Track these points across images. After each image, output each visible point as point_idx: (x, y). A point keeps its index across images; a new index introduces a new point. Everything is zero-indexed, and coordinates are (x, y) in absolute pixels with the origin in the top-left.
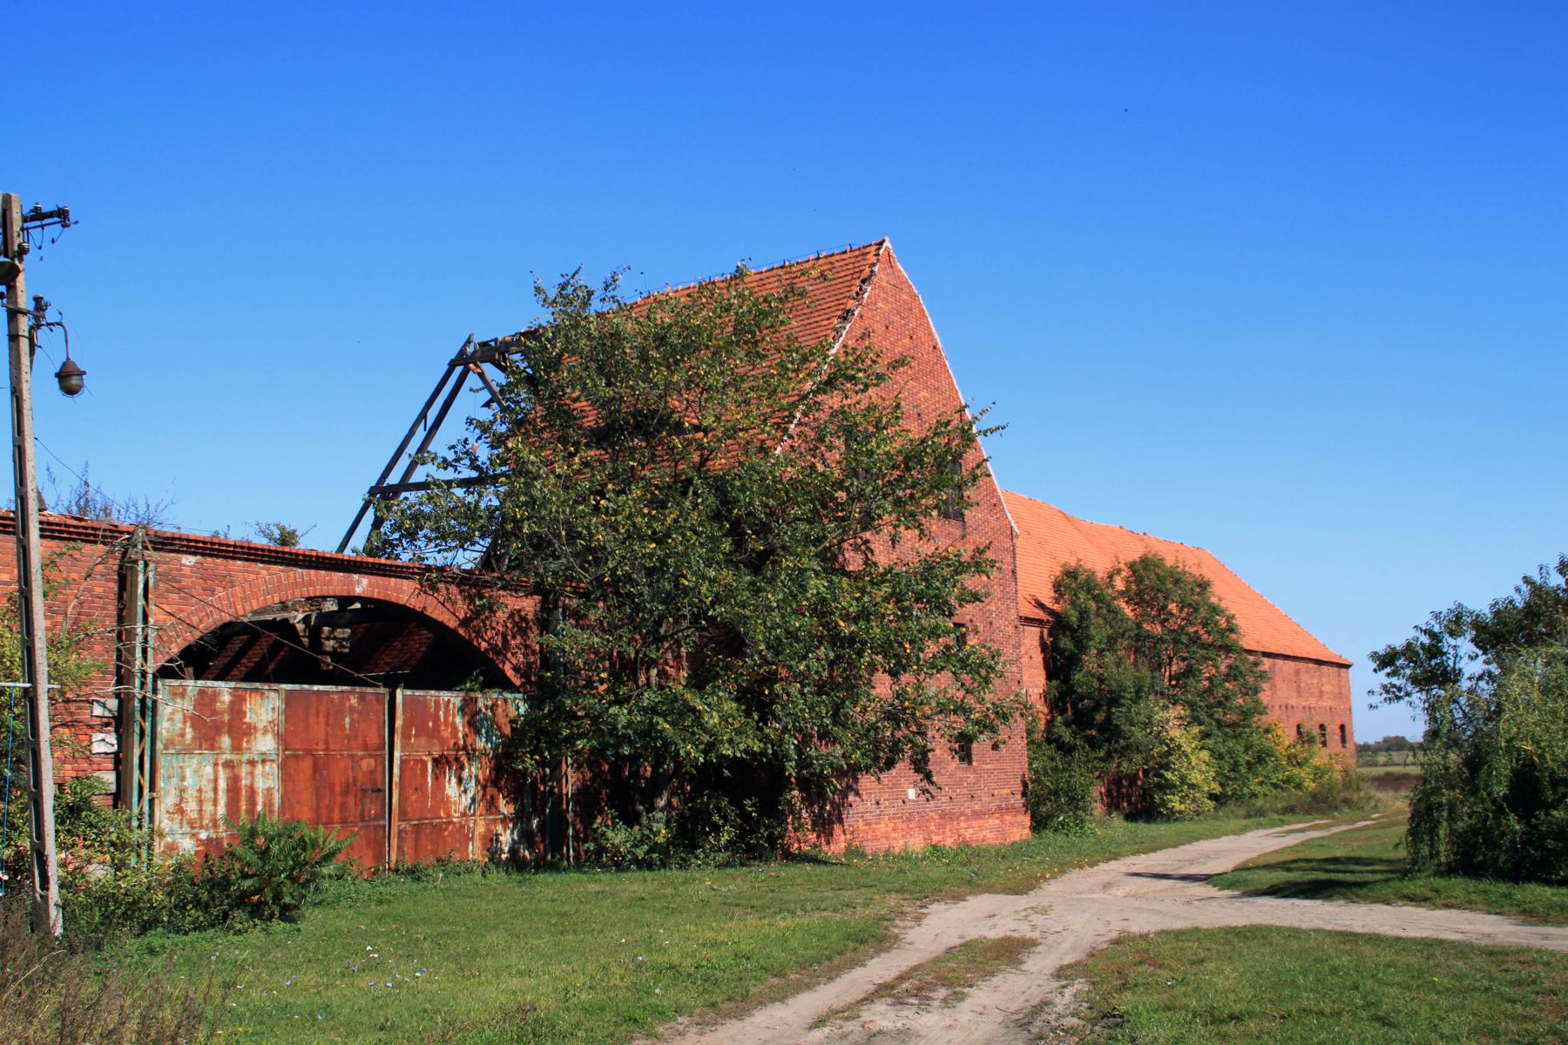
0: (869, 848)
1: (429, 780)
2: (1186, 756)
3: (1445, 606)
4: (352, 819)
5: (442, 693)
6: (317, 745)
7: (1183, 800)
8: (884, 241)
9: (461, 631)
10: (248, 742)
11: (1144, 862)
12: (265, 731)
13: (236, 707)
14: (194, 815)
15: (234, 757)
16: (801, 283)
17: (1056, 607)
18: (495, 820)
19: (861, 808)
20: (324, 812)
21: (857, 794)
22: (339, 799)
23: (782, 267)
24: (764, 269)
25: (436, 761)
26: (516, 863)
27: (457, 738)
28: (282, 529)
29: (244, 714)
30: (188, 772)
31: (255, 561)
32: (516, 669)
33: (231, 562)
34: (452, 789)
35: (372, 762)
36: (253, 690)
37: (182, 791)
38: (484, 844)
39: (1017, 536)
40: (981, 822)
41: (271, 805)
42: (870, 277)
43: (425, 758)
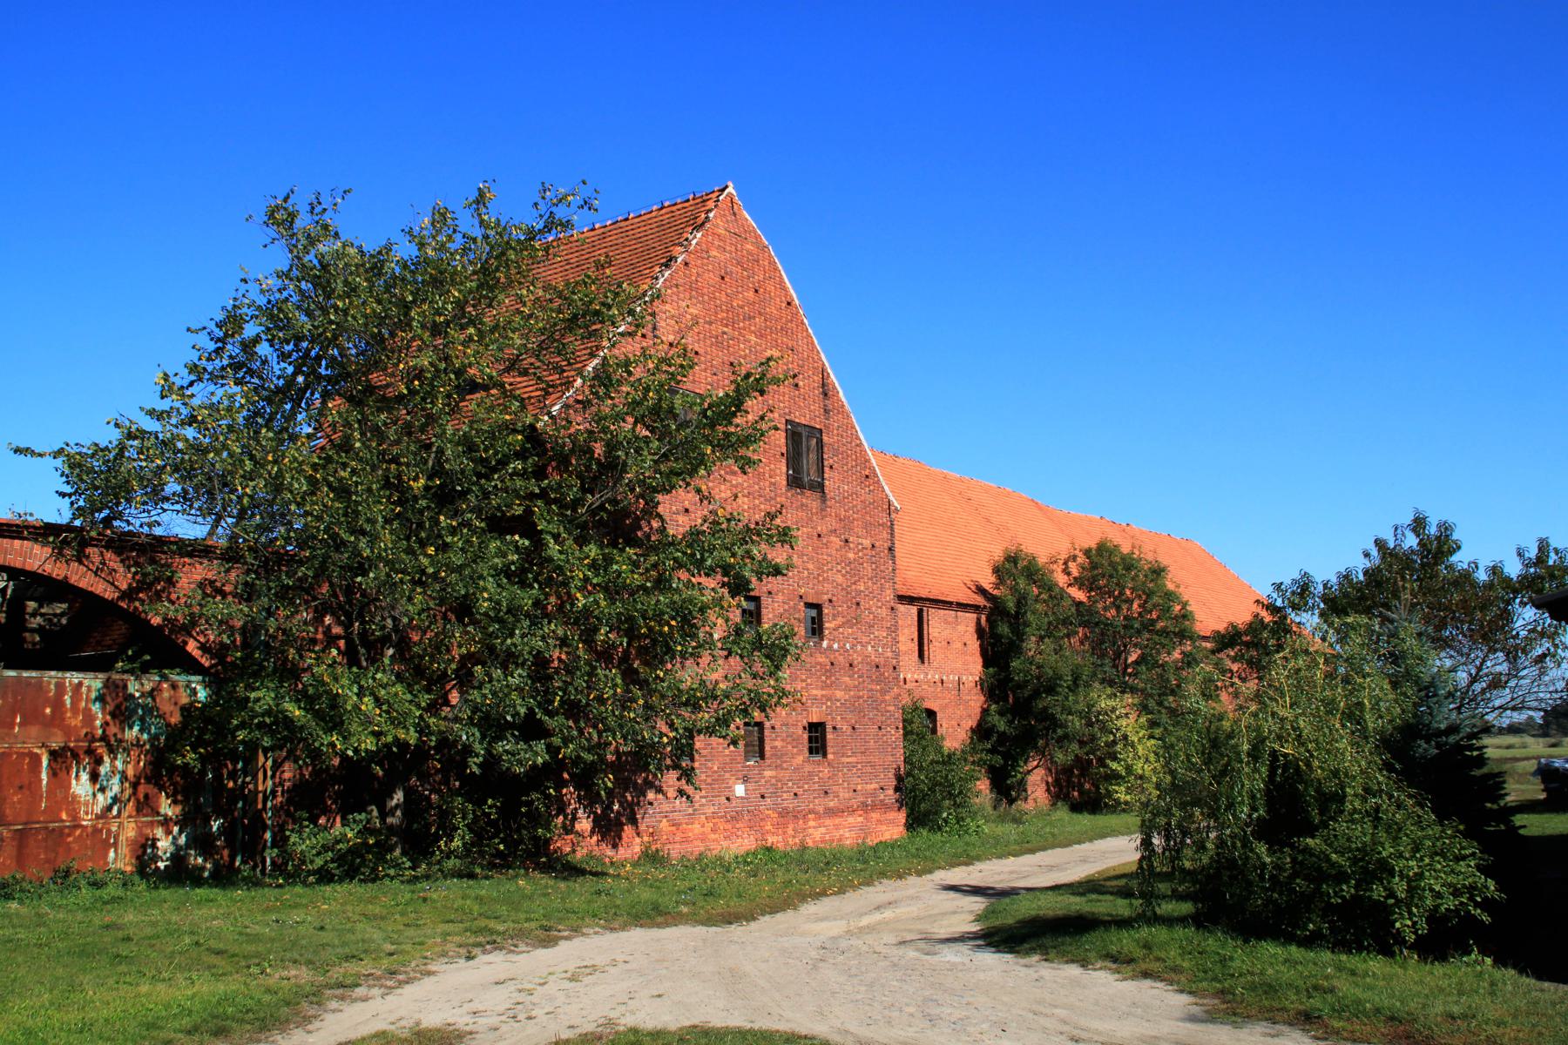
0: (675, 851)
1: (44, 776)
2: (1133, 746)
3: (1288, 576)
5: (68, 675)
7: (1129, 791)
8: (727, 187)
11: (958, 875)
16: (561, 213)
17: (996, 592)
18: (152, 823)
19: (666, 807)
23: (627, 219)
24: (609, 223)
25: (54, 755)
26: (179, 873)
27: (93, 728)
32: (204, 648)
34: (81, 786)
38: (133, 851)
39: (896, 510)
40: (837, 821)
42: (703, 224)
43: (37, 751)
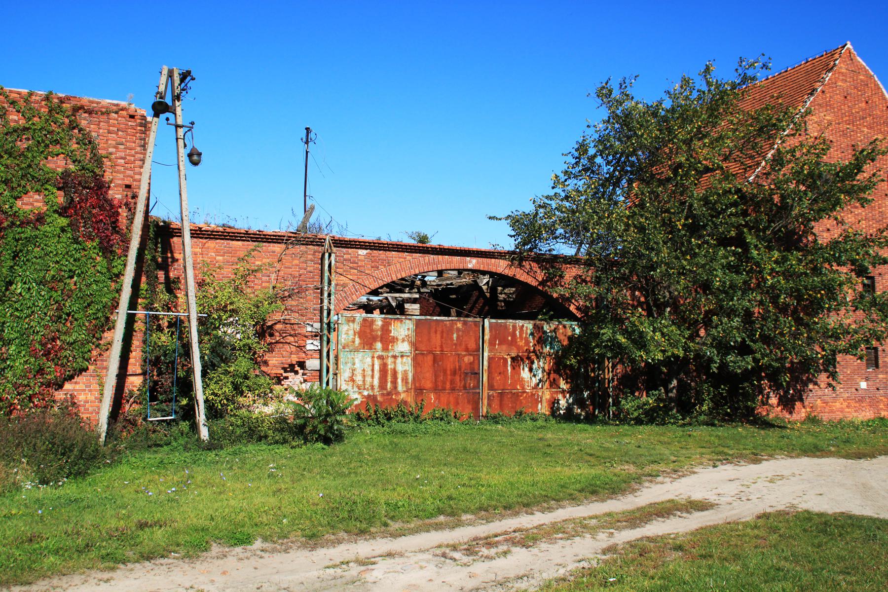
0: (825, 417)
1: (509, 368)
4: (458, 388)
5: (517, 321)
6: (436, 348)
8: (846, 45)
9: (540, 288)
10: (392, 346)
12: (403, 341)
13: (385, 328)
14: (360, 383)
15: (384, 354)
20: (440, 384)
21: (816, 384)
22: (449, 377)
23: (786, 71)
25: (513, 359)
26: (569, 417)
27: (529, 346)
28: (419, 235)
29: (391, 331)
30: (357, 361)
31: (404, 252)
32: (578, 308)
33: (388, 252)
34: (525, 374)
35: (472, 358)
36: (395, 319)
37: (353, 370)
41: (407, 379)
42: (832, 68)
43: (506, 357)
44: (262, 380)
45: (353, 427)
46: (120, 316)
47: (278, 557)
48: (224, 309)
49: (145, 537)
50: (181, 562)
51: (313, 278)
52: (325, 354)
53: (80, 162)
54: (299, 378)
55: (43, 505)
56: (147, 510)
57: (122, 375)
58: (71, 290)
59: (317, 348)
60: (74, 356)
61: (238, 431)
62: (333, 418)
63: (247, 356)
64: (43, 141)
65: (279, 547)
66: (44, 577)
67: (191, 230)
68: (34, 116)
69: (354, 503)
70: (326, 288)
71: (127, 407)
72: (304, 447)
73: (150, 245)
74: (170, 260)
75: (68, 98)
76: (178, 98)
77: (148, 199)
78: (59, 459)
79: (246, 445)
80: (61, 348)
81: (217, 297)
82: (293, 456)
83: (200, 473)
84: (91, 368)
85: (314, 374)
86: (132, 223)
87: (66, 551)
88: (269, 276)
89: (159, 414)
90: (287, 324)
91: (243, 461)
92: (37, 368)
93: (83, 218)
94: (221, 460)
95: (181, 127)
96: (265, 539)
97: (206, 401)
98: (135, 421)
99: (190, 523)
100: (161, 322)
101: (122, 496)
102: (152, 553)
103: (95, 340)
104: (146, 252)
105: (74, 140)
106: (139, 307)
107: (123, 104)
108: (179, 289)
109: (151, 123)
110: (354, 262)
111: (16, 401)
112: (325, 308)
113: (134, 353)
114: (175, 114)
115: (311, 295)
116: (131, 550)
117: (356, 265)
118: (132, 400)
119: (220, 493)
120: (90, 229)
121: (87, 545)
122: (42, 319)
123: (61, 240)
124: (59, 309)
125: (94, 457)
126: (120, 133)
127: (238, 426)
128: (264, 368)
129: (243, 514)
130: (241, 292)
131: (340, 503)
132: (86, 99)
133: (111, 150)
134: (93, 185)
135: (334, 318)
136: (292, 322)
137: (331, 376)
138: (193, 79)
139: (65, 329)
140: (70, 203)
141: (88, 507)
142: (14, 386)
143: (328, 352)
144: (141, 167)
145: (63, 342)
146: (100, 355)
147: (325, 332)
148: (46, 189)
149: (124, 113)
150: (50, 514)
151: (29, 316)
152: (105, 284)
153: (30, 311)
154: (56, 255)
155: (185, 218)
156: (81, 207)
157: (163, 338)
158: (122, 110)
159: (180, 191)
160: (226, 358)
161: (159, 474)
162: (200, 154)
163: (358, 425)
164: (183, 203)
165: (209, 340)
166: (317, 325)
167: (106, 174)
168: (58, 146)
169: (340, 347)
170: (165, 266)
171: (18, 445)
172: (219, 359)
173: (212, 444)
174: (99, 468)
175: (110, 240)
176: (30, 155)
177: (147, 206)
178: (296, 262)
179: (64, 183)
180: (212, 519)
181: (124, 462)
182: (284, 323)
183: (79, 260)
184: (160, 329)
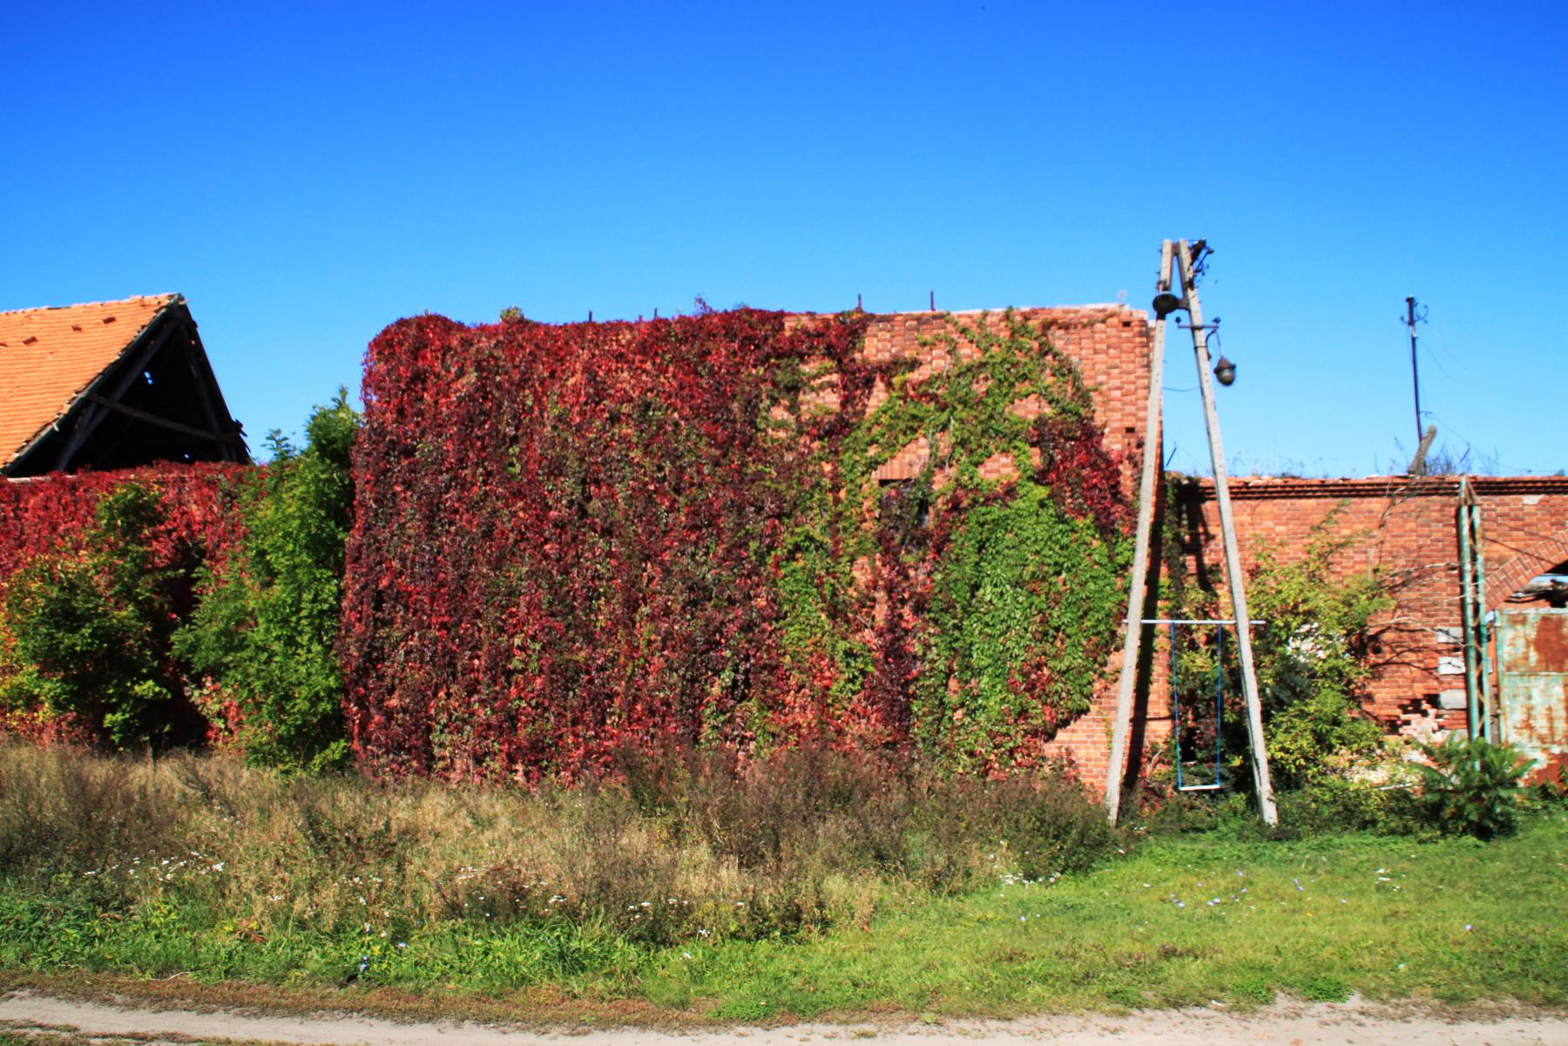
14: (1545, 731)
30: (1535, 692)
37: (1530, 708)
44: (1362, 727)
45: (1535, 811)
46: (1130, 627)
47: (1389, 1029)
48: (1294, 611)
49: (1172, 971)
50: (1226, 1017)
51: (1443, 550)
52: (1473, 681)
53: (1058, 402)
54: (1430, 722)
55: (1029, 909)
56: (1177, 931)
57: (1139, 720)
58: (1058, 593)
59: (1458, 671)
60: (1068, 692)
61: (1326, 812)
62: (1493, 794)
63: (1337, 687)
64: (1006, 379)
65: (1391, 1010)
66: (1028, 1013)
67: (1231, 488)
68: (991, 345)
69: (1533, 947)
70: (1468, 567)
71: (1149, 768)
72: (1441, 842)
73: (1170, 516)
74: (1202, 537)
75: (1035, 312)
76: (1190, 284)
77: (1161, 445)
78: (1051, 844)
79: (1339, 835)
80: (1050, 680)
81: (1280, 592)
82: (1422, 857)
83: (1263, 876)
84: (1094, 708)
85: (1456, 716)
86: (1140, 484)
87: (1057, 979)
88: (1365, 552)
89: (1197, 780)
90: (1402, 631)
91: (1335, 861)
92: (1019, 709)
93: (1068, 484)
94: (1298, 857)
95: (1200, 328)
96: (1367, 994)
97: (1272, 761)
98: (1161, 789)
99: (1242, 955)
100: (1194, 636)
101: (1141, 906)
102: (1182, 998)
103: (1096, 666)
104: (1165, 528)
105: (1048, 371)
106: (1160, 614)
107: (1112, 306)
108: (1220, 581)
109: (1154, 329)
110: (1517, 519)
111: (992, 757)
112: (1469, 600)
113: (1155, 685)
114: (1188, 310)
115: (1441, 579)
116: (1151, 989)
117: (1520, 523)
118: (1155, 758)
119: (1294, 911)
120: (1081, 500)
121: (1087, 975)
122: (1022, 637)
123: (1041, 519)
124: (1044, 622)
125: (1101, 844)
126: (1112, 351)
127: (1326, 803)
128: (1367, 707)
129: (1329, 949)
130: (1321, 581)
131: (1505, 945)
132: (1058, 307)
133: (1101, 378)
134: (1079, 433)
135: (1486, 617)
136: (1412, 627)
137: (1487, 718)
138: (1210, 252)
139: (1053, 651)
140: (1049, 464)
141: (1091, 918)
142: (989, 735)
143: (1480, 678)
144: (1146, 398)
145: (1052, 669)
146: (1106, 688)
147: (1472, 643)
148: (1015, 448)
149: (1114, 321)
150: (1038, 923)
151: (1003, 633)
152: (1107, 581)
153: (1004, 627)
154: (1035, 542)
155: (1218, 470)
156: (1065, 468)
157: (1199, 662)
158: (1111, 316)
159: (1208, 429)
160: (1301, 692)
161: (1198, 875)
162: (1232, 368)
163: (1545, 808)
164: (1215, 447)
165: (1273, 663)
166: (1457, 632)
167: (1096, 415)
168: (1027, 383)
169: (1501, 668)
170: (1195, 548)
171: (996, 821)
172: (1289, 693)
173: (1284, 831)
174: (1109, 860)
175: (1109, 514)
176: (990, 401)
177: (1161, 456)
178: (1411, 525)
179: (1039, 435)
180: (1278, 952)
181: (1145, 853)
182: (1397, 629)
183: (1067, 547)
184: (1193, 646)
